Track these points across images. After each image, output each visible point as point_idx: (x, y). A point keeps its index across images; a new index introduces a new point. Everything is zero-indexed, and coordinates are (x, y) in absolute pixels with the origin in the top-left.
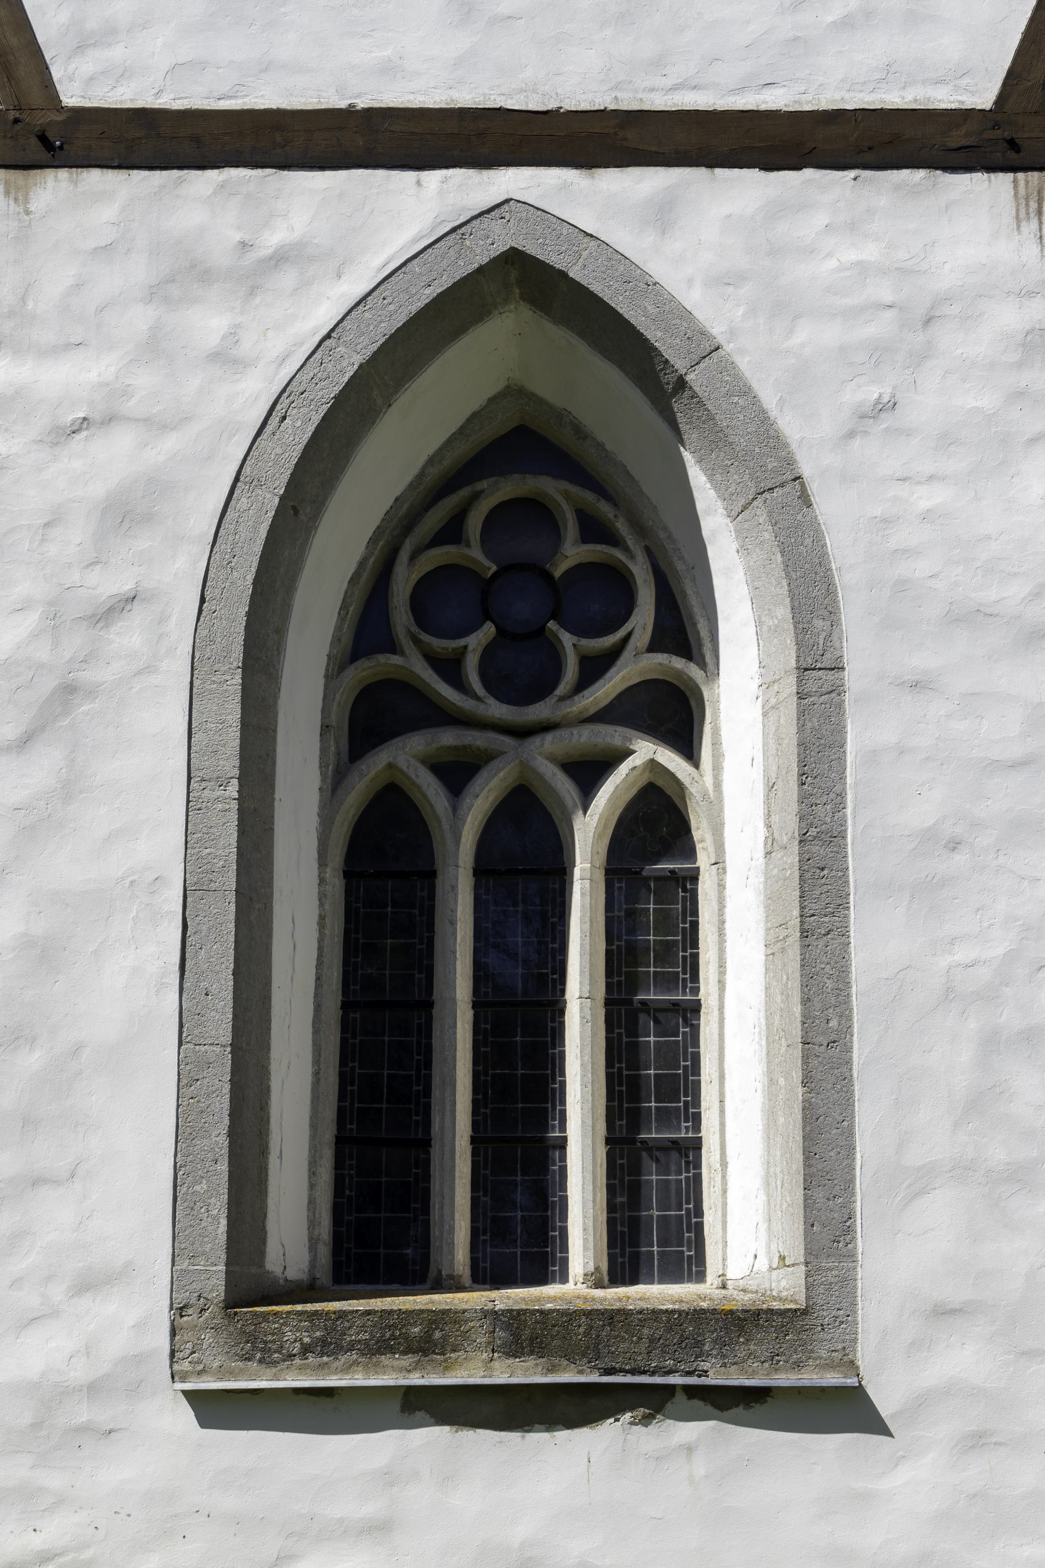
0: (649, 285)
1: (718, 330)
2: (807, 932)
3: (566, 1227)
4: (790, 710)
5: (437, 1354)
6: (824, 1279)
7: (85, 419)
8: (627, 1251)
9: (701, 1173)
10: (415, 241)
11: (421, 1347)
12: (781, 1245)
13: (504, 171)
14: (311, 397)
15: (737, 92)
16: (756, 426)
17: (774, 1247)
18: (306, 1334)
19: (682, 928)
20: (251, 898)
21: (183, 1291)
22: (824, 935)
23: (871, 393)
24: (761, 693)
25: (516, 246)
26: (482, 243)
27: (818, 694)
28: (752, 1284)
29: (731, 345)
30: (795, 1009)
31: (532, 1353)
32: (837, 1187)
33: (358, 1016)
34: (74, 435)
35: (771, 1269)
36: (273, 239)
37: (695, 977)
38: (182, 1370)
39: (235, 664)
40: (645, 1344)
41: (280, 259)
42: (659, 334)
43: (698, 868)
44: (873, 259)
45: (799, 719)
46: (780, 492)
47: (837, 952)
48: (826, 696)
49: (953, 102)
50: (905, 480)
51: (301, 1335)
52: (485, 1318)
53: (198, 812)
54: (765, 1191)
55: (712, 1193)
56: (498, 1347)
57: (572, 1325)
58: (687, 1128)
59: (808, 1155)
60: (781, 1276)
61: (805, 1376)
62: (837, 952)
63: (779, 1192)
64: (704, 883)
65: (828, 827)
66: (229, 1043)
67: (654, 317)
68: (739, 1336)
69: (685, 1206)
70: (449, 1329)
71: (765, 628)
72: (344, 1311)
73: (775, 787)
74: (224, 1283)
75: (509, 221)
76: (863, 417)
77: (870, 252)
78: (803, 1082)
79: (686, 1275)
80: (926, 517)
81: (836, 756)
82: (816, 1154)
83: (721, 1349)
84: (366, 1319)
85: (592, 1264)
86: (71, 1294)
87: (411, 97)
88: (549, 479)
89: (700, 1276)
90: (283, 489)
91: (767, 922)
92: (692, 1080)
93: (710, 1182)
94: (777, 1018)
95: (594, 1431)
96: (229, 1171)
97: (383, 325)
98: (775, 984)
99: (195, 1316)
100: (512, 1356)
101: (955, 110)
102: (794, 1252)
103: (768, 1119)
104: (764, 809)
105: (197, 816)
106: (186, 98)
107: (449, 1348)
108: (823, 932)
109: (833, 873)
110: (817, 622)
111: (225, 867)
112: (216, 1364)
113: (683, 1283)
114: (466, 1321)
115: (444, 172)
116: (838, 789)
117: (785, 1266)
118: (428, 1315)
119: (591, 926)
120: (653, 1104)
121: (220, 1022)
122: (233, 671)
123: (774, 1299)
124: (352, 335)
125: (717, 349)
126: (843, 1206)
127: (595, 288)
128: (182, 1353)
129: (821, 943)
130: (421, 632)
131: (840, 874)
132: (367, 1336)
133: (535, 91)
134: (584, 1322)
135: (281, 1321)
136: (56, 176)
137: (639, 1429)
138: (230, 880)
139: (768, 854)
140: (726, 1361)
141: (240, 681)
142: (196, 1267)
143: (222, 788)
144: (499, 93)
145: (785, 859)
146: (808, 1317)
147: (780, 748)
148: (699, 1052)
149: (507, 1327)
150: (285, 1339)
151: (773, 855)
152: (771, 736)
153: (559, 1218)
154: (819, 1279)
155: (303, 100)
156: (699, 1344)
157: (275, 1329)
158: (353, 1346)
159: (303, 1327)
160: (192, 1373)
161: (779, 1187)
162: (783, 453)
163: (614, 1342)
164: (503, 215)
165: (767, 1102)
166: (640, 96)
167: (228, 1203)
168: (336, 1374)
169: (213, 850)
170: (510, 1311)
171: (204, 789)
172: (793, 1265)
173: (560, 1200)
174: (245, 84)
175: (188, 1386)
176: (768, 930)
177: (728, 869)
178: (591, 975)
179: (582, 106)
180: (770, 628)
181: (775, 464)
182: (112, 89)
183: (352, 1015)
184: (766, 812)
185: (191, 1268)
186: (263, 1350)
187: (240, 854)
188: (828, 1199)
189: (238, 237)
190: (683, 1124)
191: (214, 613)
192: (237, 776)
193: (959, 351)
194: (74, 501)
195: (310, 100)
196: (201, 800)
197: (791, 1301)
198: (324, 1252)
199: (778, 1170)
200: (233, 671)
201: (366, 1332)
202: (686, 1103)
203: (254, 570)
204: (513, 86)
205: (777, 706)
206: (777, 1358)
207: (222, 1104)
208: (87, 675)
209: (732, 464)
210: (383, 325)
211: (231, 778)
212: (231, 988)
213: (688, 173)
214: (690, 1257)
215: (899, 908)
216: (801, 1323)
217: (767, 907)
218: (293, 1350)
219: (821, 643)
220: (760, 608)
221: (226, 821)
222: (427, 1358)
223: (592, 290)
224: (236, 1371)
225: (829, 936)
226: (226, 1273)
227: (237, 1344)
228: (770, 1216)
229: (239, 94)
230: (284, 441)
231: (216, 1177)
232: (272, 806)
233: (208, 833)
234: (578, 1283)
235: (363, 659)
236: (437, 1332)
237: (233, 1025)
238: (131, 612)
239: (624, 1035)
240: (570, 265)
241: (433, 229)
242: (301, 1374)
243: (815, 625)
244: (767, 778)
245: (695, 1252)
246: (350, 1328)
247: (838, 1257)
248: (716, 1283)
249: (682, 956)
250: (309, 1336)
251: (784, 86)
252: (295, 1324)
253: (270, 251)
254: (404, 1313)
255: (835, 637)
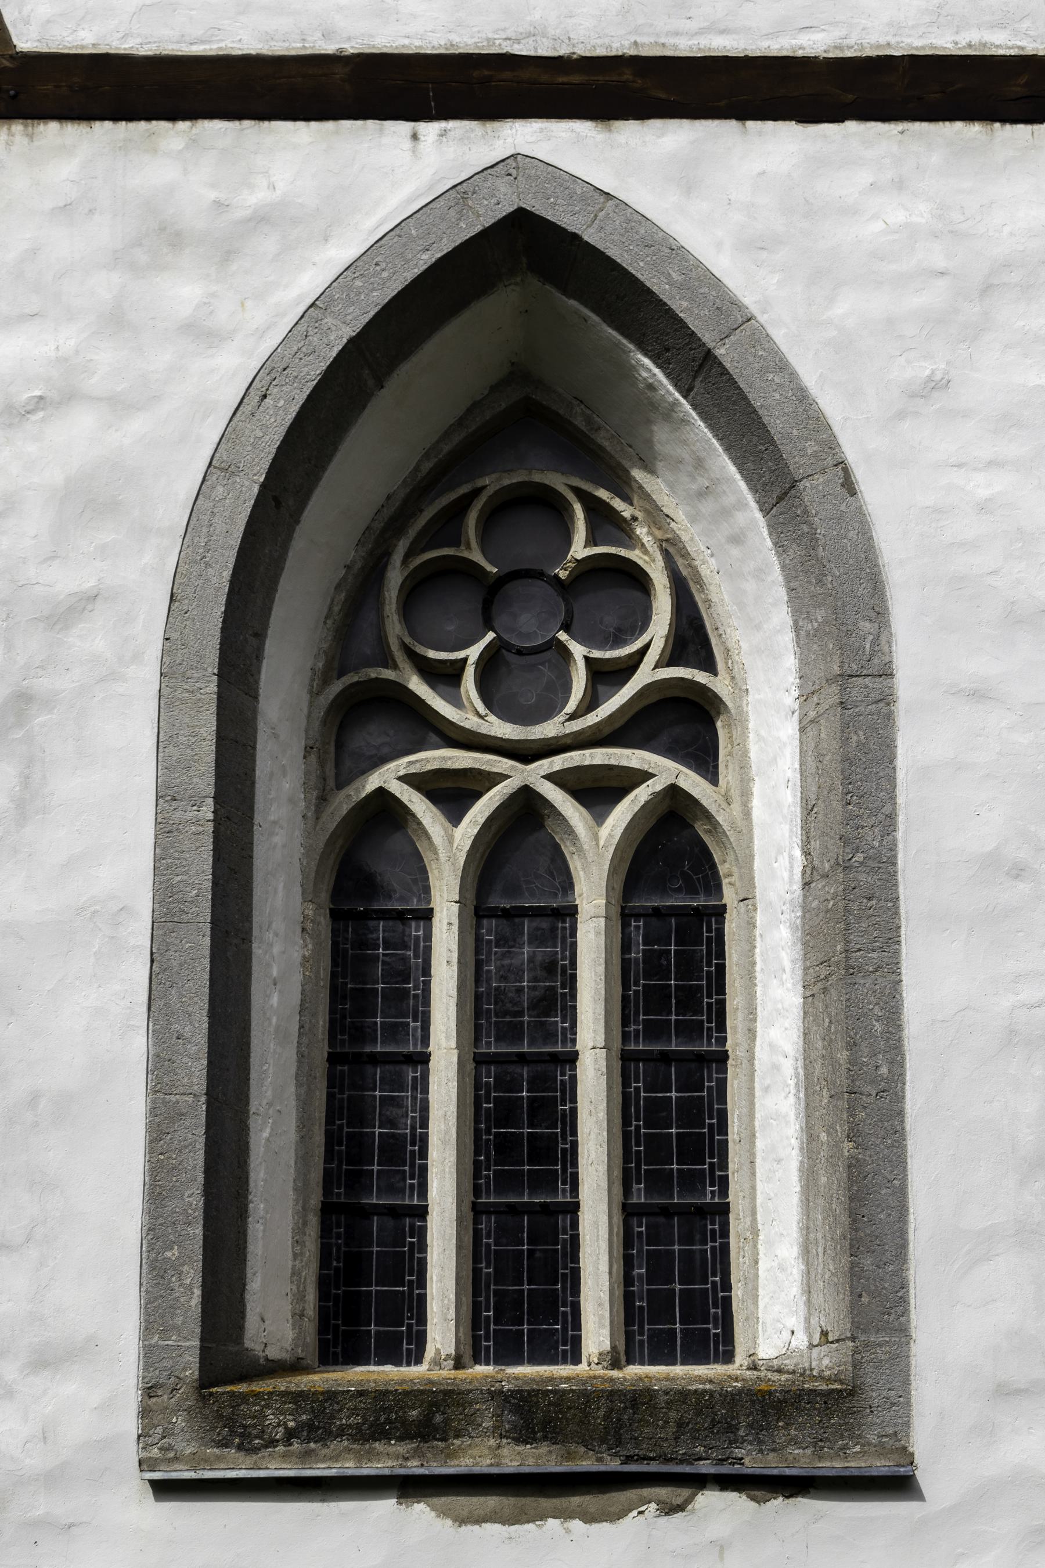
0: (673, 250)
1: (749, 300)
2: (853, 969)
3: (579, 1302)
4: (827, 730)
5: (438, 1440)
6: (873, 1356)
7: (41, 398)
8: (646, 1329)
9: (728, 1243)
10: (410, 201)
11: (420, 1432)
12: (823, 1319)
13: (510, 124)
14: (295, 374)
15: (770, 36)
16: (794, 406)
17: (814, 1321)
18: (291, 1417)
19: (707, 971)
20: (227, 932)
21: (152, 1369)
22: (873, 972)
23: (924, 369)
24: (797, 707)
25: (524, 206)
26: (486, 202)
27: (865, 704)
28: (789, 1364)
29: (765, 316)
30: (839, 1055)
31: (545, 1438)
32: (888, 1254)
33: (346, 1068)
34: (29, 416)
35: (811, 1346)
36: (255, 198)
37: (722, 1026)
38: (150, 1458)
39: (210, 670)
40: (672, 1428)
41: (261, 219)
42: (685, 304)
43: (725, 905)
44: (923, 221)
45: (843, 731)
46: (821, 480)
47: (887, 991)
48: (874, 706)
49: (1012, 48)
50: (960, 466)
51: (285, 1418)
52: (492, 1400)
53: (168, 835)
54: (803, 1259)
55: (741, 1265)
56: (506, 1431)
57: (590, 1407)
58: (712, 1192)
59: (855, 1218)
60: (823, 1354)
61: (853, 1464)
62: (887, 991)
63: (820, 1260)
64: (731, 921)
65: (876, 851)
66: (204, 1092)
67: (679, 285)
68: (778, 1420)
69: (710, 1279)
70: (452, 1412)
71: (803, 633)
72: (334, 1392)
73: (815, 810)
74: (198, 1360)
75: (515, 178)
76: (913, 396)
77: (921, 213)
78: (848, 1137)
79: (712, 1356)
80: (984, 508)
81: (885, 772)
82: (863, 1216)
83: (757, 1434)
84: (358, 1400)
85: (609, 1343)
86: (25, 1372)
87: (406, 42)
88: (559, 475)
89: (729, 1357)
90: (264, 476)
91: (805, 960)
92: (718, 1140)
93: (739, 1252)
94: (818, 1067)
95: (615, 1526)
96: (204, 1235)
97: (375, 294)
98: (815, 1028)
99: (166, 1397)
100: (522, 1442)
101: (1014, 56)
102: (838, 1326)
103: (808, 1180)
104: (802, 835)
105: (167, 839)
106: (155, 42)
107: (452, 1434)
108: (871, 969)
109: (882, 903)
110: (862, 623)
111: (198, 896)
112: (189, 1451)
113: (708, 1363)
114: (471, 1404)
115: (443, 124)
116: (887, 809)
117: (828, 1342)
118: (428, 1397)
119: (606, 968)
120: (675, 1166)
121: (193, 1069)
122: (208, 679)
123: (814, 1378)
124: (340, 306)
125: (749, 320)
126: (894, 1274)
127: (613, 252)
128: (151, 1439)
129: (869, 982)
130: (416, 643)
131: (890, 904)
132: (359, 1419)
133: (544, 35)
134: (603, 1404)
135: (263, 1403)
136: (9, 129)
137: (664, 1520)
138: (204, 912)
139: (806, 885)
140: (764, 1448)
141: (216, 689)
142: (167, 1343)
143: (195, 808)
144: (504, 37)
145: (827, 889)
146: (855, 1398)
147: (820, 765)
148: (726, 1109)
149: (517, 1410)
150: (267, 1423)
151: (813, 885)
152: (810, 753)
153: (571, 1293)
154: (867, 1356)
155: (286, 45)
156: (732, 1429)
157: (255, 1411)
158: (343, 1430)
159: (288, 1409)
160: (162, 1460)
161: (821, 1255)
162: (824, 436)
163: (637, 1427)
164: (509, 172)
165: (806, 1161)
166: (662, 40)
167: (203, 1271)
168: (323, 1462)
169: (185, 878)
170: (520, 1391)
171: (175, 809)
172: (838, 1341)
173: (572, 1272)
174: (221, 27)
175: (157, 1476)
176: (806, 969)
177: (758, 905)
178: (606, 1022)
179: (598, 51)
180: (808, 633)
181: (815, 449)
182: (72, 34)
183: (339, 1068)
184: (804, 838)
185: (161, 1343)
186: (242, 1435)
187: (215, 883)
188: (878, 1267)
189: (213, 195)
190: (709, 1189)
191: (186, 613)
192: (212, 795)
193: (1022, 323)
194: (29, 489)
195: (294, 45)
196: (171, 822)
197: (835, 1381)
198: (310, 1327)
199: (819, 1235)
200: (208, 679)
201: (358, 1415)
202: (712, 1165)
203: (231, 566)
204: (521, 30)
205: (817, 720)
206: (820, 1443)
207: (197, 1159)
208: (43, 684)
209: (766, 450)
210: (375, 294)
211: (206, 797)
212: (205, 1031)
213: (717, 126)
214: (716, 1335)
215: (956, 942)
216: (847, 1405)
217: (805, 944)
218: (276, 1435)
219: (868, 646)
220: (797, 612)
221: (200, 845)
222: (426, 1445)
223: (609, 254)
224: (212, 1459)
225: (878, 974)
226: (201, 1349)
227: (214, 1428)
228: (809, 1287)
229: (214, 38)
230: (264, 422)
231: (188, 1242)
232: (250, 832)
233: (179, 859)
234: (593, 1364)
235: (352, 674)
236: (437, 1414)
237: (208, 1072)
238: (92, 613)
239: (642, 1090)
240: (585, 227)
241: (431, 188)
242: (285, 1462)
243: (861, 628)
244: (805, 799)
245: (722, 1330)
246: (340, 1410)
247: (888, 1331)
248: (746, 1364)
249: (707, 1002)
250: (294, 1420)
251: (824, 30)
252: (278, 1406)
253: (249, 212)
254: (400, 1393)
255: (883, 640)
